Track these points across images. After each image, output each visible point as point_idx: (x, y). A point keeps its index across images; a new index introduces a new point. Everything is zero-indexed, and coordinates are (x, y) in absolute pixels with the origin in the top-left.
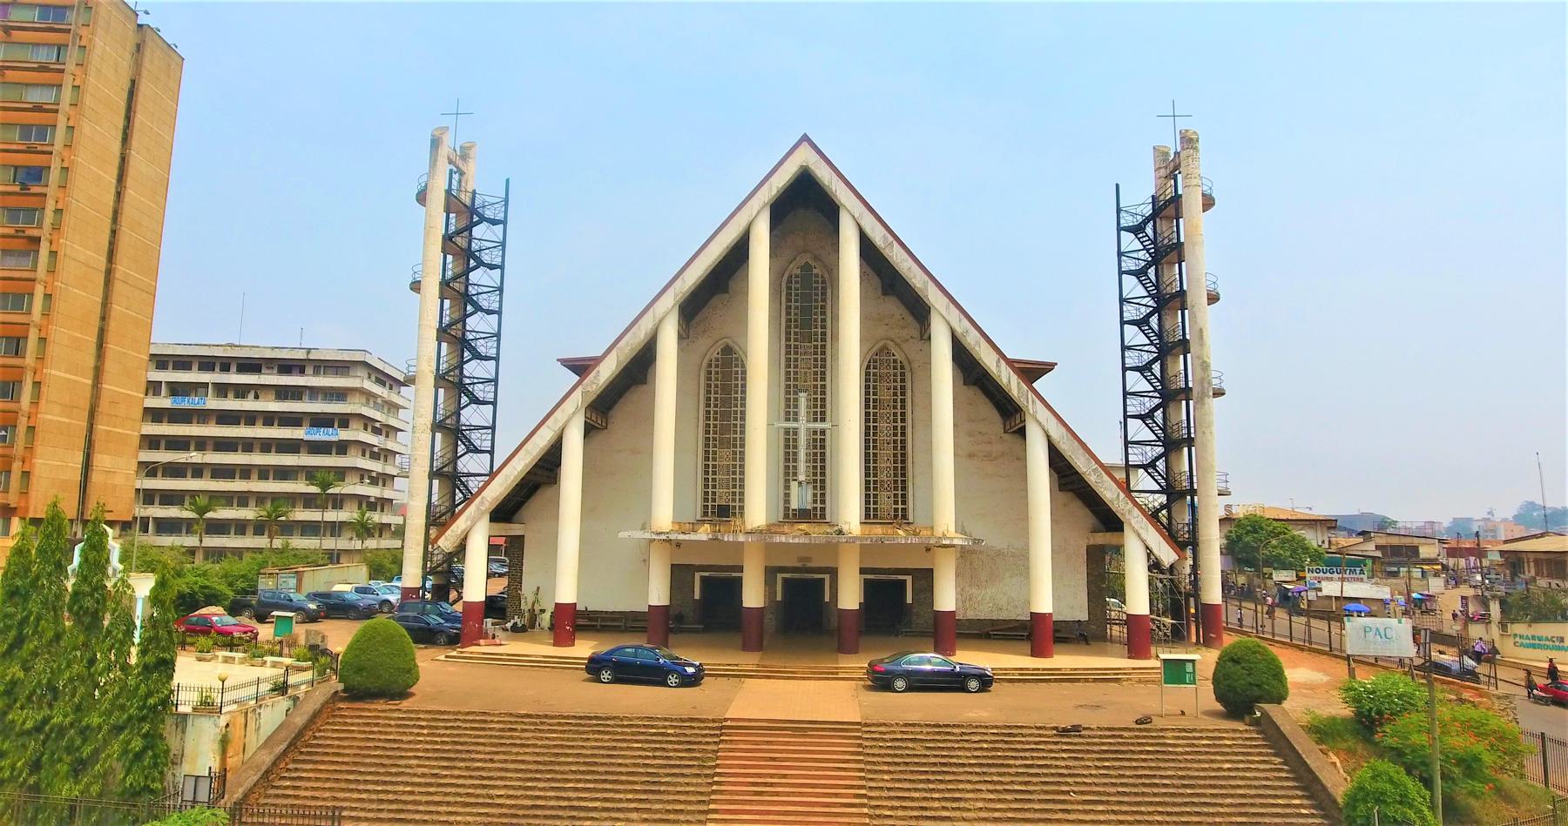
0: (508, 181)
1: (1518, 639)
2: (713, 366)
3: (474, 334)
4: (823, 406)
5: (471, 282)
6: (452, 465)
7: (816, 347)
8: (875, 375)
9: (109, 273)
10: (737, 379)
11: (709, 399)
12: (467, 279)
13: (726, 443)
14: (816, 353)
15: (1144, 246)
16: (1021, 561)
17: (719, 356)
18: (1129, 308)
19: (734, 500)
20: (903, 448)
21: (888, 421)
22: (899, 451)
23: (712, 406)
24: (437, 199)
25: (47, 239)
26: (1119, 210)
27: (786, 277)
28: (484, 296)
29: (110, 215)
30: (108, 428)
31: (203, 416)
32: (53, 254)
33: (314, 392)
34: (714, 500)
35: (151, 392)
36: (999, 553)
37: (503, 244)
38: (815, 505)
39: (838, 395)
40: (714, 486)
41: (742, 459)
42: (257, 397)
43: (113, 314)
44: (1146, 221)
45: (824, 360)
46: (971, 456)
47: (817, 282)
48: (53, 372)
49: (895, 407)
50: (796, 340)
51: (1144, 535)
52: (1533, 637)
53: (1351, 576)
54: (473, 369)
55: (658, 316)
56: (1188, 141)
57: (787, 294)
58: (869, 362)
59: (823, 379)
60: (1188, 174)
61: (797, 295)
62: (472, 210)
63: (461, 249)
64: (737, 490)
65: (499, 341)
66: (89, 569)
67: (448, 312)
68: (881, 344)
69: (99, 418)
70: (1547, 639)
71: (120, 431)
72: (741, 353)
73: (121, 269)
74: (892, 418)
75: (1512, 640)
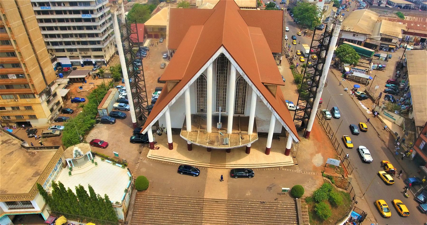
7: (225, 76)
8: (239, 83)
11: (198, 87)
20: (245, 99)
29: (15, 4)
30: (43, 62)
31: (52, 12)
32: (10, 28)
34: (200, 108)
35: (34, 6)
36: (264, 121)
39: (229, 95)
42: (64, 5)
43: (30, 33)
45: (226, 79)
48: (31, 71)
49: (244, 90)
51: (293, 137)
52: (388, 114)
55: (185, 91)
57: (217, 62)
59: (226, 84)
69: (40, 61)
70: (390, 115)
72: (205, 76)
73: (25, 19)
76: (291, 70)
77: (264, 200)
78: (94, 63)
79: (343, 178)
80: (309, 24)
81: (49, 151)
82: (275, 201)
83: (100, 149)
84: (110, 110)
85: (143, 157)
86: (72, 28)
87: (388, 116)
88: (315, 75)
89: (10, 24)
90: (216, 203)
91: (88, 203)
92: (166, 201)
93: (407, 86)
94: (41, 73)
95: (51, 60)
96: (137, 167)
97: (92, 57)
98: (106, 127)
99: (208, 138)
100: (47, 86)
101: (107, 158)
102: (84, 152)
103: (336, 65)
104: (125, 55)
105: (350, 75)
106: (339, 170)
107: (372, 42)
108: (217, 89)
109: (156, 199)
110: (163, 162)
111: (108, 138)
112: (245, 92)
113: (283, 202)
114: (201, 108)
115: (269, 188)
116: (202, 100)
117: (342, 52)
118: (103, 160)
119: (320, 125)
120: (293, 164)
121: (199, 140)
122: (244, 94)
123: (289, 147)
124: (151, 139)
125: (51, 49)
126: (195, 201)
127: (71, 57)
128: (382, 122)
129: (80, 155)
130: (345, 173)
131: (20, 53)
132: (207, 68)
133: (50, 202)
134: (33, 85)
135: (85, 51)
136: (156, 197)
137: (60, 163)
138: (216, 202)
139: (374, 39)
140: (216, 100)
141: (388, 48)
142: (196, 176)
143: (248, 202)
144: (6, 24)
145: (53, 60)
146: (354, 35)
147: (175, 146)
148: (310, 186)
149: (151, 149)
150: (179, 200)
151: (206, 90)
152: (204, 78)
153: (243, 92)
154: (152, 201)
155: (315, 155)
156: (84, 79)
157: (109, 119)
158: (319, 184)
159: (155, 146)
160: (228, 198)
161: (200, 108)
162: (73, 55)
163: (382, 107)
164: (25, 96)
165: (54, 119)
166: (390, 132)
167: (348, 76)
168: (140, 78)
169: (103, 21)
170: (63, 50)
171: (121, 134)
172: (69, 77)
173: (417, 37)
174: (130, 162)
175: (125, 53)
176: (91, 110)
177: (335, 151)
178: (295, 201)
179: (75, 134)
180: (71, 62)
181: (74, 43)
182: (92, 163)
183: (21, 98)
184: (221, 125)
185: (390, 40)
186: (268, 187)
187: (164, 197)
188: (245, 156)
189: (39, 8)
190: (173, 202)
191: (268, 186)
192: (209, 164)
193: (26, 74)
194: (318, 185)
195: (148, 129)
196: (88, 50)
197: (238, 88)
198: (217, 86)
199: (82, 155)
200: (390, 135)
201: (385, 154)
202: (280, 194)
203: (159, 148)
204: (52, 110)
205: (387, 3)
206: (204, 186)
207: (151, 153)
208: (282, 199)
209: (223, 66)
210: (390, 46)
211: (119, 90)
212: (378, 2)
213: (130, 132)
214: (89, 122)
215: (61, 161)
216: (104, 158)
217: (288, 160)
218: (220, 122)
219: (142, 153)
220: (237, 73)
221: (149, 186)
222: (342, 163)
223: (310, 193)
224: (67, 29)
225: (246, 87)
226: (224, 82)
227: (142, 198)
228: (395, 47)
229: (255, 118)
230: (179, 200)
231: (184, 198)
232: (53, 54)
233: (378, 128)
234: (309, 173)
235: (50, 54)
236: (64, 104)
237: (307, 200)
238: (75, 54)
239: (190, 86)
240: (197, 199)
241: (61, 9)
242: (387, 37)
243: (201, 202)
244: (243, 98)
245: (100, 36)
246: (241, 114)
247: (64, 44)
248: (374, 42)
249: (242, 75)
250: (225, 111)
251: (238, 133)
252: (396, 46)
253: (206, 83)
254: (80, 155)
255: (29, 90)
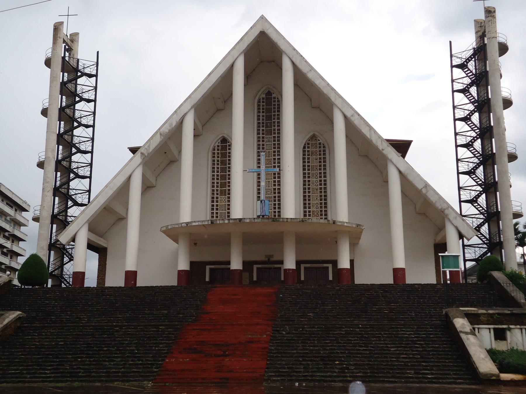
0: (98, 52)
2: (216, 150)
3: (74, 191)
5: (72, 161)
6: (60, 269)
7: (274, 137)
12: (69, 186)
13: (223, 193)
15: (467, 74)
17: (220, 144)
18: (463, 165)
20: (325, 192)
21: (316, 177)
23: (215, 179)
24: (57, 64)
26: (451, 56)
28: (79, 195)
32: (329, 148)
37: (91, 165)
38: (277, 167)
44: (468, 60)
47: (275, 101)
50: (263, 134)
56: (490, 12)
58: (305, 145)
60: (489, 31)
61: (263, 109)
62: (77, 70)
63: (70, 91)
65: (93, 142)
67: (59, 179)
209: (269, 118)
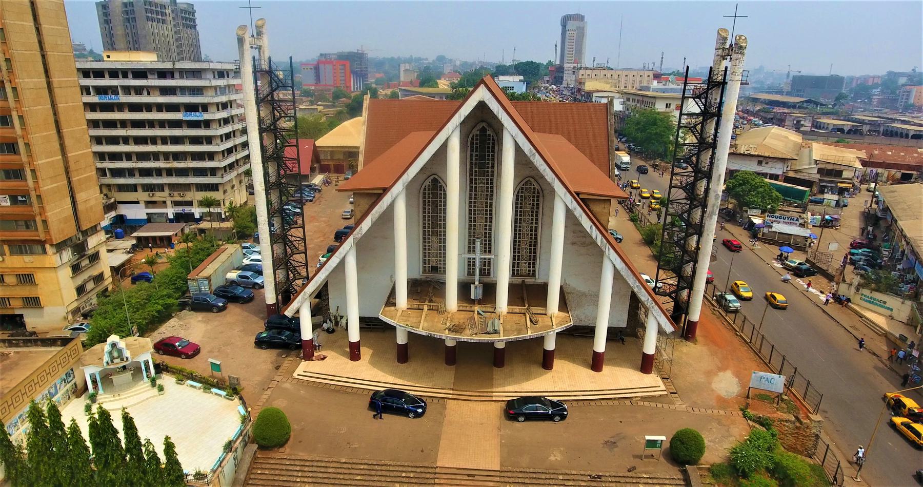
1: (863, 296)
4: (491, 214)
7: (487, 179)
8: (522, 196)
9: (49, 84)
10: (441, 198)
13: (435, 233)
14: (487, 183)
16: (595, 298)
19: (440, 264)
20: (536, 238)
22: (533, 240)
25: (7, 81)
27: (471, 136)
30: (79, 178)
31: (120, 107)
32: (14, 89)
33: (183, 90)
34: (429, 264)
35: (85, 93)
36: (584, 294)
39: (498, 235)
40: (429, 257)
41: (445, 243)
42: (149, 94)
43: (64, 134)
45: (492, 188)
46: (573, 244)
48: (40, 162)
49: (532, 216)
51: (658, 318)
52: (871, 298)
53: (791, 221)
54: (281, 95)
55: (394, 196)
59: (491, 199)
64: (442, 259)
66: (130, 438)
68: (527, 179)
70: (878, 300)
71: (85, 175)
72: (441, 181)
73: (55, 80)
74: (530, 221)
75: (860, 296)
76: (632, 223)
77: (601, 471)
78: (197, 216)
79: (798, 424)
80: (661, 150)
81: (46, 351)
82: (630, 474)
83: (179, 359)
84: (217, 282)
85: (282, 377)
86: (159, 141)
87: (873, 303)
88: (679, 288)
89: (16, 80)
90: (470, 478)
91: (117, 467)
92: (334, 476)
93: (900, 251)
94: (69, 200)
95: (104, 207)
96: (266, 397)
97: (195, 203)
98: (203, 318)
99: (449, 319)
100: (80, 234)
101: (192, 377)
102: (134, 354)
103: (727, 216)
104: (263, 162)
105: (766, 230)
106: (784, 405)
107: (801, 175)
108: (470, 214)
109: (306, 469)
110: (333, 387)
111: (203, 338)
112: (537, 220)
113: (652, 476)
114: (433, 262)
115: (611, 444)
116: (434, 240)
117: (740, 184)
118: (180, 381)
119: (718, 318)
120: (665, 393)
121: (426, 325)
122: (534, 225)
123: (650, 347)
124: (307, 333)
125: (109, 186)
126: (412, 475)
127: (149, 204)
128: (861, 316)
129: (122, 360)
130: (801, 412)
131: (27, 145)
132: (447, 140)
133: (17, 470)
134: (45, 222)
135: (182, 191)
136: (307, 464)
137: (69, 383)
138: (469, 476)
139: (803, 171)
140: (467, 240)
141: (837, 190)
142: (418, 415)
143: (555, 476)
144: (8, 79)
145: (109, 208)
146: (760, 163)
147: (366, 352)
148: (717, 440)
149: (306, 360)
150: (367, 472)
151: (445, 217)
152: (441, 186)
153: (532, 219)
154: (295, 473)
155: (717, 375)
156: (169, 239)
157: (212, 299)
158: (741, 435)
159: (316, 354)
160: (502, 465)
161: (429, 264)
162: (154, 199)
163: (856, 283)
164: (23, 248)
165: (82, 311)
166: (886, 335)
167: (761, 233)
168: (297, 245)
169: (229, 144)
170: (133, 188)
171: (235, 330)
172: (135, 234)
173: (893, 171)
174: (248, 385)
175: (265, 160)
176: (170, 281)
177: (765, 366)
178: (685, 473)
179: (121, 321)
180: (147, 214)
181: (159, 172)
182: (150, 388)
183: (12, 254)
184: (481, 292)
185: (839, 173)
186: (606, 442)
187: (328, 465)
188: (542, 375)
189: (94, 99)
190: (353, 477)
191: (606, 440)
192: (451, 392)
193: (33, 194)
194: (738, 437)
195: (302, 303)
196: (187, 187)
197: (519, 210)
198: (470, 206)
199: (127, 358)
200: (887, 343)
201: (887, 383)
202: (640, 457)
203: (325, 358)
204: (80, 290)
205: (813, 124)
206: (438, 438)
207: (304, 368)
208: (647, 469)
209: (482, 157)
210: (839, 184)
211: (244, 251)
212: (795, 122)
213: (259, 327)
214: (160, 301)
215: (72, 376)
216: (183, 376)
217: (652, 382)
218: (477, 283)
219: (282, 368)
220: (518, 149)
221: (291, 439)
222: (788, 388)
223: (720, 455)
224: (149, 142)
225: (538, 208)
226: (487, 195)
227: (268, 466)
228: (851, 185)
229: (561, 287)
230: (367, 472)
231: (383, 468)
232: (110, 196)
233: (855, 328)
234: (709, 411)
235: (105, 195)
236: (113, 283)
237: (715, 471)
238: (158, 196)
239: (406, 186)
240: (418, 470)
241: (141, 99)
242: (830, 167)
243: (428, 476)
244: (531, 235)
245: (214, 142)
246: (529, 275)
247: (137, 174)
248: (804, 176)
249: (529, 155)
250: (490, 252)
251: (523, 311)
252: (854, 185)
253: (445, 198)
254: (122, 360)
255: (11, 130)
